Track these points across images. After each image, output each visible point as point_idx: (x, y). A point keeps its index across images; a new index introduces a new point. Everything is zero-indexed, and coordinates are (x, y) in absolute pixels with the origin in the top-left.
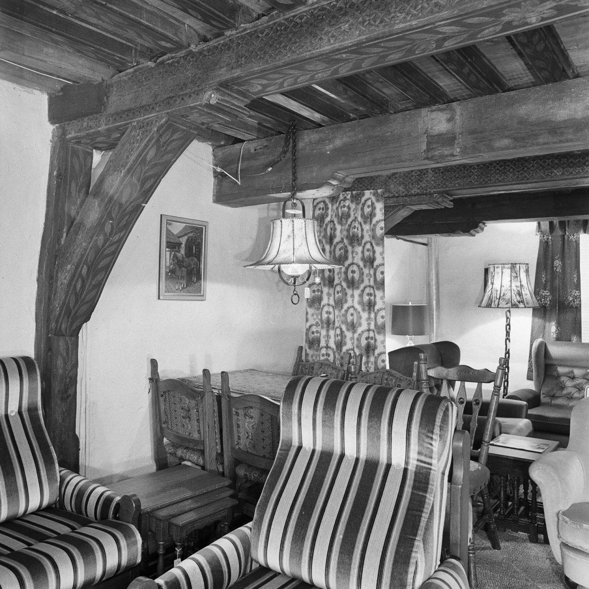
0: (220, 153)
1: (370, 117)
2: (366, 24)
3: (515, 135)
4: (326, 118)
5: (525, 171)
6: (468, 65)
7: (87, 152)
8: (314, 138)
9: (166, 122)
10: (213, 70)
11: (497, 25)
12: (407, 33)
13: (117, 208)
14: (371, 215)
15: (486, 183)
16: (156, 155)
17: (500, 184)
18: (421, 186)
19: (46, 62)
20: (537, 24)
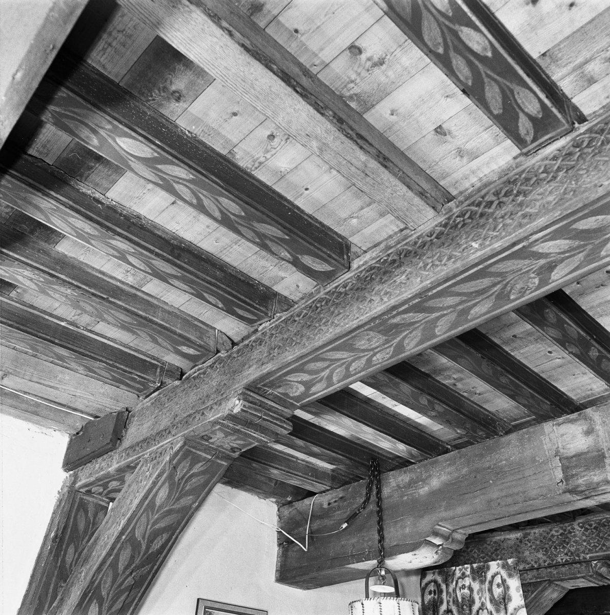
0: (286, 512)
1: (473, 444)
2: (428, 267)
4: (414, 451)
6: (597, 345)
7: (100, 505)
8: (402, 480)
9: (181, 448)
10: (241, 371)
13: (109, 580)
14: (504, 599)
16: (169, 497)
19: (57, 389)
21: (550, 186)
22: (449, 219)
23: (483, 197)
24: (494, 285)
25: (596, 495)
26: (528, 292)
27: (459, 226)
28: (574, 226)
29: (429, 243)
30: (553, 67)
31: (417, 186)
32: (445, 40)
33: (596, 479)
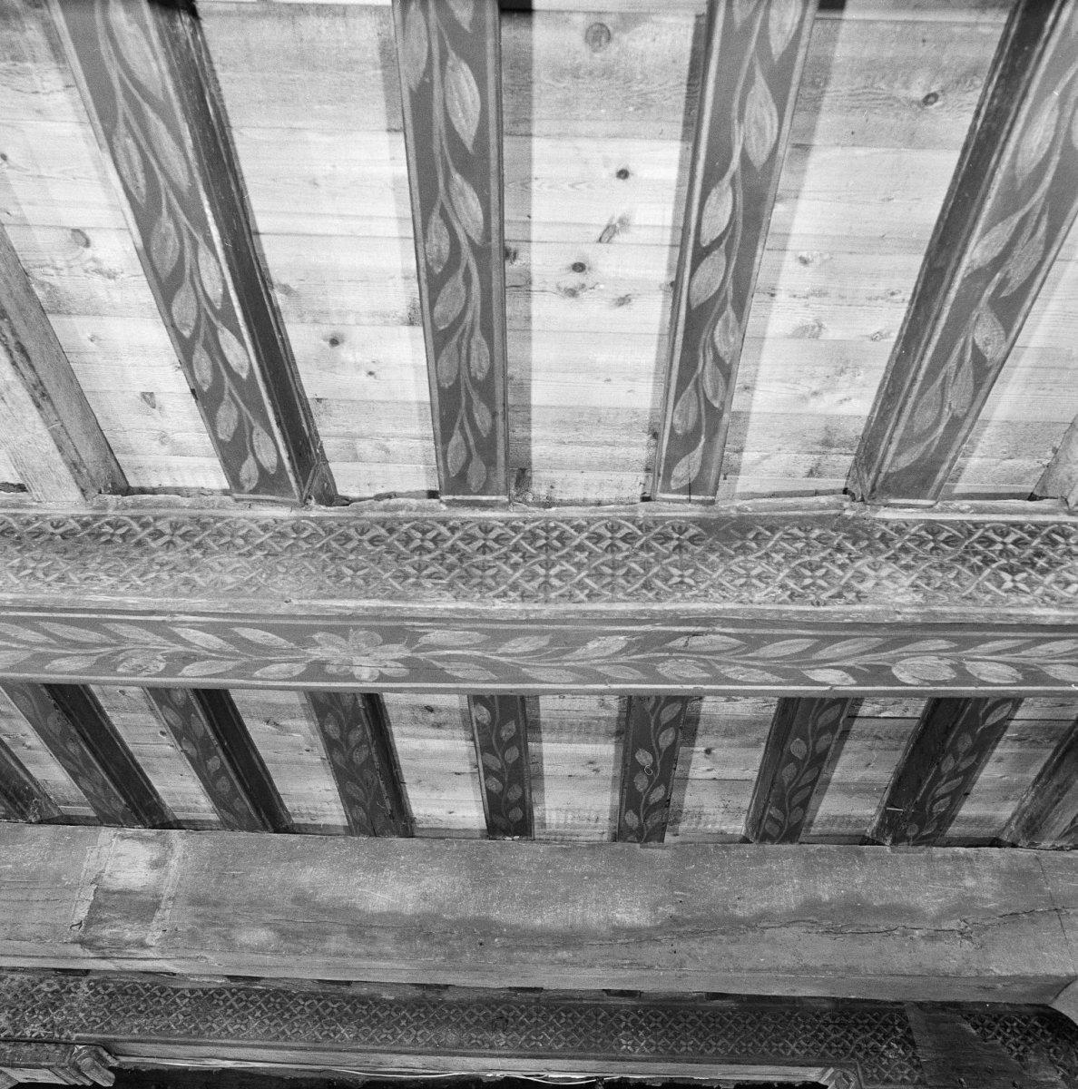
3: (285, 923)
5: (286, 1021)
6: (223, 757)
11: (296, 661)
12: (109, 616)
15: (201, 1034)
17: (228, 1041)
18: (52, 1021)
20: (370, 685)
21: (239, 562)
22: (96, 518)
23: (156, 519)
24: (104, 645)
25: (118, 958)
26: (144, 673)
27: (103, 539)
28: (236, 630)
29: (47, 537)
30: (323, 418)
31: (73, 452)
32: (197, 327)
33: (129, 936)
